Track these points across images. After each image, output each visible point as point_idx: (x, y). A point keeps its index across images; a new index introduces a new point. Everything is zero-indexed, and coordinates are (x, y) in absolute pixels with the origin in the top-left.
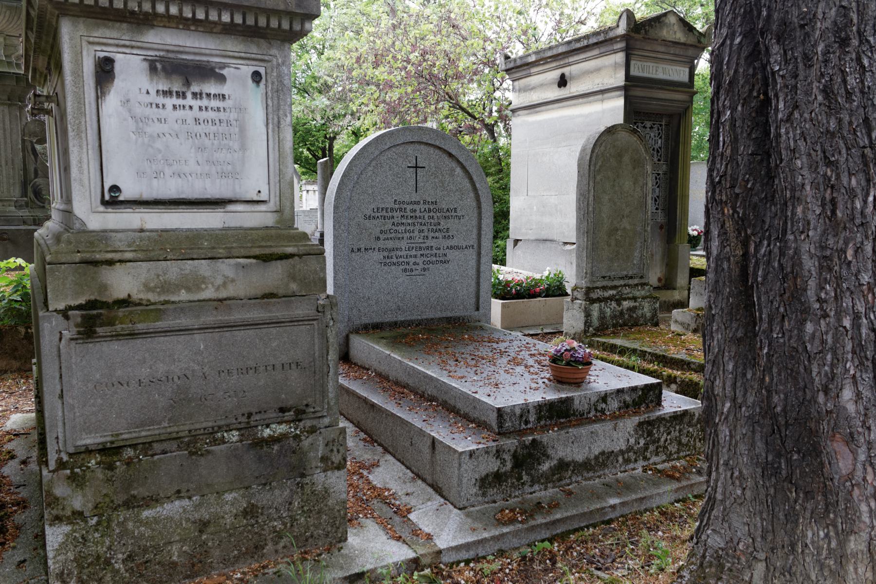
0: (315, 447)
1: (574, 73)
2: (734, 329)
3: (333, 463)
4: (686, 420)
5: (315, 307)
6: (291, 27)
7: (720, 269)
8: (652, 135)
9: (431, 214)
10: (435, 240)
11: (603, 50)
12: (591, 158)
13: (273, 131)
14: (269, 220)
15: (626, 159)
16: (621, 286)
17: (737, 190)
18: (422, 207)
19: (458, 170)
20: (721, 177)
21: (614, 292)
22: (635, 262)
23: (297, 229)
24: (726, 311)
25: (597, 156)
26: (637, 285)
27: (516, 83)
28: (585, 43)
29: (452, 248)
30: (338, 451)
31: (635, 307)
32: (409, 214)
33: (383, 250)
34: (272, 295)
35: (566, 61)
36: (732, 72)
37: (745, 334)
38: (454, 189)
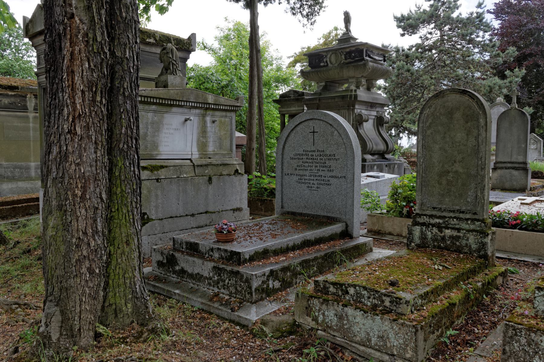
4: (239, 276)
9: (321, 157)
15: (458, 115)
18: (316, 153)
19: (336, 132)
21: (441, 221)
26: (467, 220)
29: (332, 177)
31: (459, 237)
33: (299, 175)
38: (334, 143)
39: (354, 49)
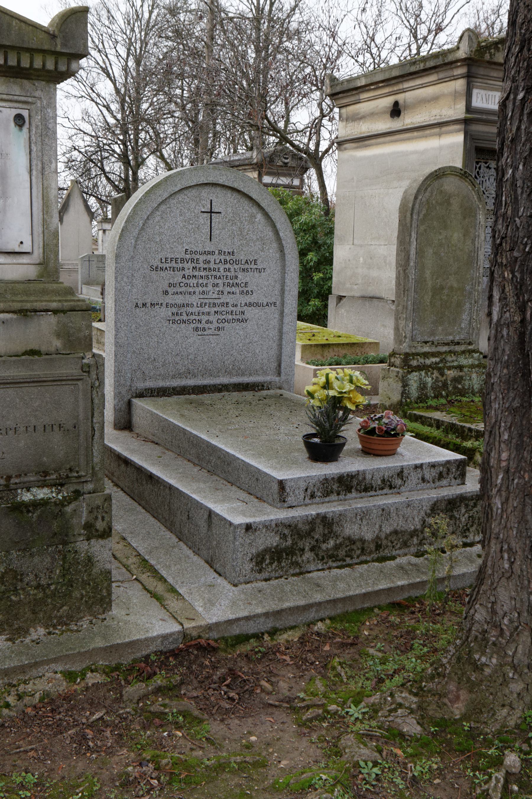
0: (80, 513)
1: (409, 101)
2: (511, 399)
3: (97, 530)
5: (79, 366)
6: (56, 68)
7: (499, 336)
9: (227, 266)
10: (231, 296)
11: (441, 75)
12: (414, 205)
13: (37, 178)
14: (32, 272)
16: (445, 352)
17: (516, 254)
18: (217, 257)
19: (259, 216)
20: (503, 238)
21: (438, 360)
22: (463, 325)
23: (62, 283)
24: (503, 380)
25: (421, 203)
26: (463, 352)
27: (344, 110)
28: (422, 66)
29: (250, 305)
30: (103, 519)
31: (461, 377)
32: (202, 265)
33: (172, 306)
34: (33, 352)
35: (400, 86)
36: (514, 129)
37: (522, 405)
38: (255, 238)
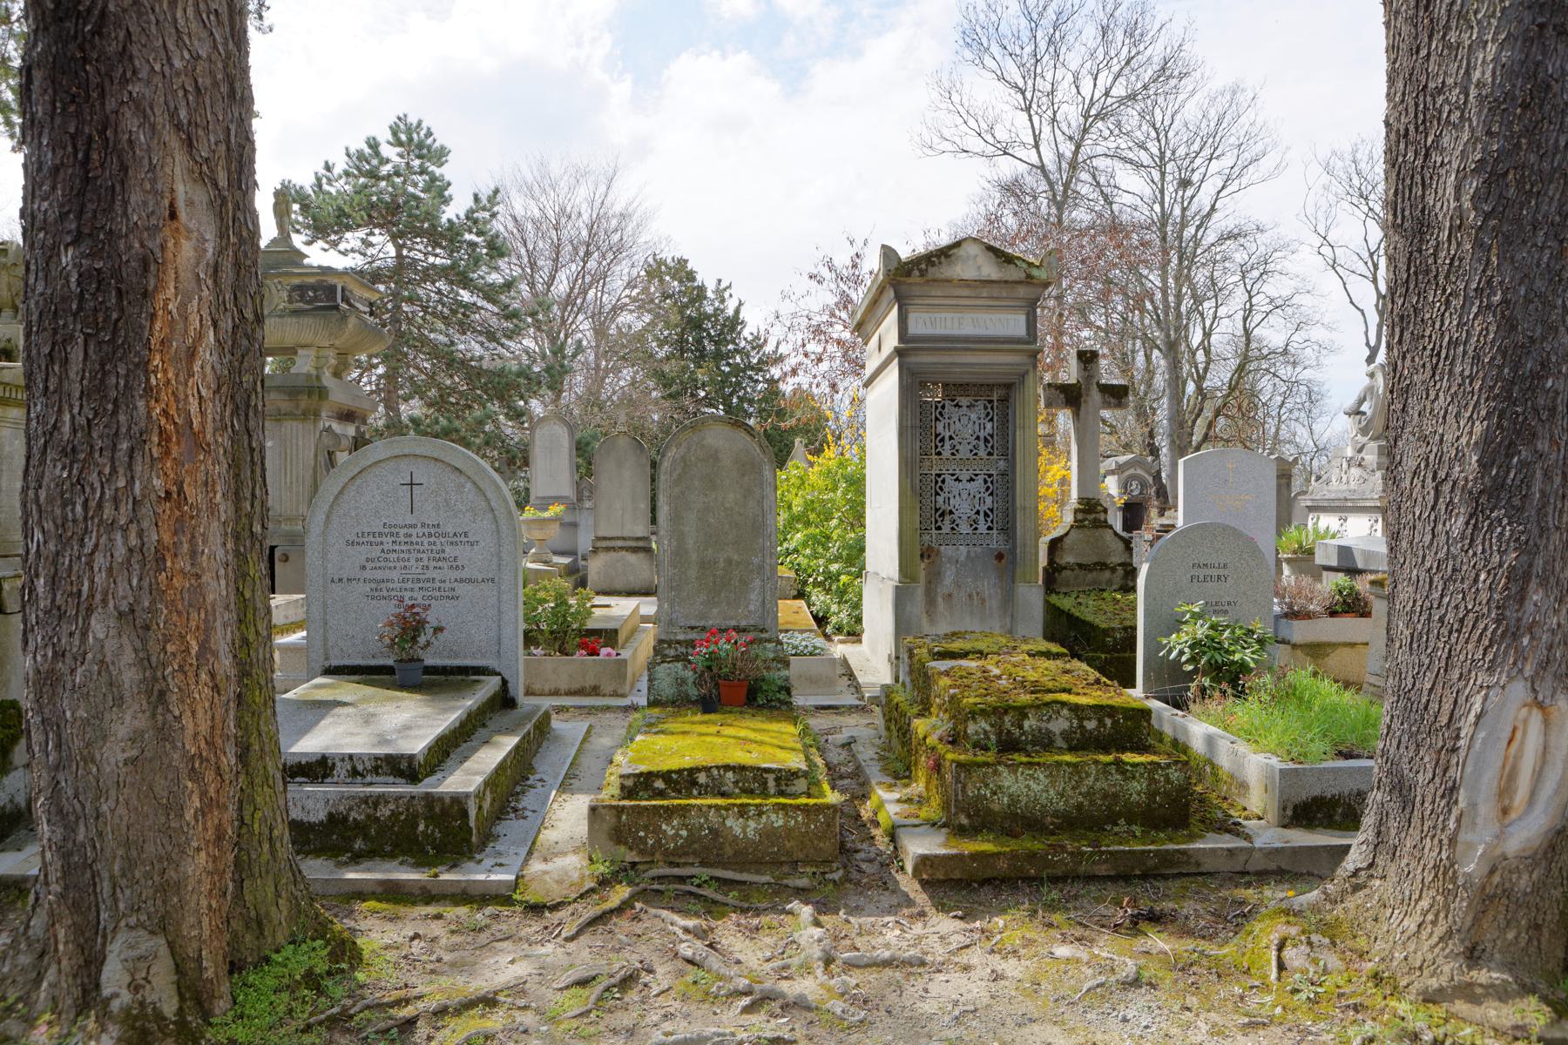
8: (974, 416)
18: (420, 530)
19: (469, 485)
29: (462, 581)
33: (371, 581)
39: (312, 280)
